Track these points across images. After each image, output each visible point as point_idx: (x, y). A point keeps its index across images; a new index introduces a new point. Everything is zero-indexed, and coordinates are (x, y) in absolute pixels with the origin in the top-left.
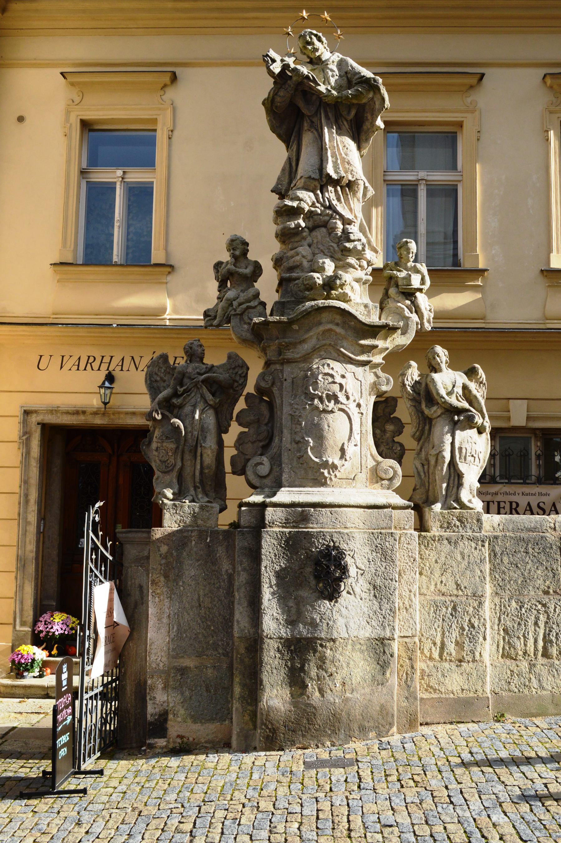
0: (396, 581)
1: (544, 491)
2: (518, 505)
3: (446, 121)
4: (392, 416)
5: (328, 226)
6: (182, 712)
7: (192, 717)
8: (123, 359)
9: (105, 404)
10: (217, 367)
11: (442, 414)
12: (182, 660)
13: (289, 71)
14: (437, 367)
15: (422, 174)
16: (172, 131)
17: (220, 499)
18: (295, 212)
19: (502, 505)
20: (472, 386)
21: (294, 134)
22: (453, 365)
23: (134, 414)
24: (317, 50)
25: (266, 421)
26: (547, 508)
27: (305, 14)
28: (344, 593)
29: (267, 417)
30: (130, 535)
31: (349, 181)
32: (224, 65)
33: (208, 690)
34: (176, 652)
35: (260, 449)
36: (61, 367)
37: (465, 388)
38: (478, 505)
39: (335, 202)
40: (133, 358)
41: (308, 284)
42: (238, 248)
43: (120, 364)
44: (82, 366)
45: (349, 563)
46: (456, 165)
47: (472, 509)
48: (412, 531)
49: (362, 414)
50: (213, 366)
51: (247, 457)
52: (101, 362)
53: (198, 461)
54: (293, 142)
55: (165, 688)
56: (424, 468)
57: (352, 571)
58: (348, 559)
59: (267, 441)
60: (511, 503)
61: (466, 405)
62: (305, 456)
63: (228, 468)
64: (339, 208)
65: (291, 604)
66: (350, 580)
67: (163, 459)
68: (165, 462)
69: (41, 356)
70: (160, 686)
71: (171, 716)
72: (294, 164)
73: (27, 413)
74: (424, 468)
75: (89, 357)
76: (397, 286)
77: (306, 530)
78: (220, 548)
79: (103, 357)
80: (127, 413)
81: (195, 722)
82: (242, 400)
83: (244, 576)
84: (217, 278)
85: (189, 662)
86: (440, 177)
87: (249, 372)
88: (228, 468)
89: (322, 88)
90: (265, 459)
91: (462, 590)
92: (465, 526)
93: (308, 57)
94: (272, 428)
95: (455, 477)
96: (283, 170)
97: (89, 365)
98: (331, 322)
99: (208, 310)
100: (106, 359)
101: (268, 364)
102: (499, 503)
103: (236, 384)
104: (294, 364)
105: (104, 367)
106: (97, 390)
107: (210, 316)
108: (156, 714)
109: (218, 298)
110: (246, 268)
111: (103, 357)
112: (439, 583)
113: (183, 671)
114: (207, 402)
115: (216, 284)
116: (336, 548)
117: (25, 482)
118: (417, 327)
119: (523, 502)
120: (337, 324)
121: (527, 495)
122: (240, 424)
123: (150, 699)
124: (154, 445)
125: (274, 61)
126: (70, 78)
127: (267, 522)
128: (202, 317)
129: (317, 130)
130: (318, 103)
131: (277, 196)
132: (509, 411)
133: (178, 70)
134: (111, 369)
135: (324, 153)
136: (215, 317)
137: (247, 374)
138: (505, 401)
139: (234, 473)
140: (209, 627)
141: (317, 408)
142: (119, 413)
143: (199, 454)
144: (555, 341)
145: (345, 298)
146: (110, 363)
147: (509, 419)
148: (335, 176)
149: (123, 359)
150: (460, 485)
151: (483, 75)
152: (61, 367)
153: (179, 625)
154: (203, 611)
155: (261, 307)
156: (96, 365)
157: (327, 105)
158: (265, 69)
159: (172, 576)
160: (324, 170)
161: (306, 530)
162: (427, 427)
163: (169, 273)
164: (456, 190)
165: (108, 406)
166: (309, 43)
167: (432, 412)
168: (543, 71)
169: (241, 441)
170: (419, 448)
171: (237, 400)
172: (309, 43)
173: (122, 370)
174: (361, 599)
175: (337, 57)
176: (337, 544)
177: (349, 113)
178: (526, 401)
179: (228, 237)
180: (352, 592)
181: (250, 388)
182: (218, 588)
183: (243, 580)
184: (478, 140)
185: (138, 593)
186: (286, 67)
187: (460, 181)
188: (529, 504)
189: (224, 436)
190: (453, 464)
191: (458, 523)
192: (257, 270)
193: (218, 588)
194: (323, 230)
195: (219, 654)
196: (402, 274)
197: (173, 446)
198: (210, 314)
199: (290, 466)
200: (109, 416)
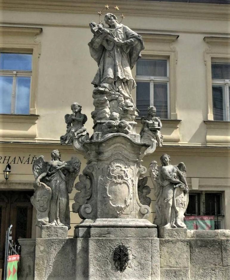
0: (150, 261)
3: (162, 55)
4: (145, 185)
5: (118, 100)
8: (15, 158)
9: (7, 179)
11: (168, 184)
13: (101, 31)
14: (166, 163)
15: (152, 78)
17: (67, 224)
18: (102, 93)
20: (181, 172)
21: (102, 58)
22: (172, 163)
23: (20, 183)
24: (114, 22)
25: (89, 188)
27: (107, 6)
28: (127, 268)
29: (89, 186)
31: (127, 80)
32: (64, 26)
35: (86, 201)
37: (178, 173)
38: (184, 225)
39: (121, 89)
41: (109, 125)
45: (129, 253)
46: (167, 74)
47: (183, 227)
48: (157, 238)
49: (133, 184)
51: (80, 204)
52: (5, 159)
53: (58, 206)
54: (101, 62)
56: (160, 209)
57: (131, 257)
58: (129, 252)
59: (89, 197)
61: (178, 180)
62: (108, 203)
63: (71, 209)
64: (123, 92)
66: (130, 261)
67: (41, 205)
68: (42, 207)
72: (102, 72)
74: (160, 209)
76: (148, 127)
77: (109, 238)
78: (68, 247)
79: (5, 157)
80: (16, 183)
82: (78, 178)
83: (80, 260)
84: (66, 122)
86: (159, 79)
87: (81, 165)
88: (71, 209)
89: (116, 39)
90: (89, 205)
91: (179, 265)
92: (179, 235)
93: (109, 25)
94: (92, 191)
95: (175, 213)
96: (97, 75)
99: (63, 136)
100: (7, 158)
101: (89, 162)
103: (76, 171)
104: (103, 162)
105: (6, 161)
106: (3, 173)
107: (63, 139)
109: (67, 131)
110: (80, 117)
111: (5, 157)
112: (168, 262)
114: (62, 179)
115: (66, 125)
116: (123, 246)
118: (157, 146)
122: (77, 189)
124: (37, 199)
125: (94, 26)
127: (91, 235)
128: (60, 140)
129: (112, 57)
130: (113, 45)
131: (94, 86)
132: (191, 183)
133: (43, 28)
134: (9, 163)
135: (116, 67)
137: (80, 166)
138: (189, 178)
139: (74, 212)
141: (114, 182)
142: (13, 183)
143: (58, 203)
145: (127, 133)
146: (9, 160)
148: (121, 78)
149: (15, 158)
150: (176, 216)
151: (178, 36)
157: (118, 46)
158: (90, 30)
160: (116, 75)
161: (109, 238)
162: (161, 190)
164: (166, 86)
165: (8, 180)
166: (109, 19)
167: (166, 183)
168: (203, 36)
169: (76, 198)
170: (158, 200)
171: (75, 178)
172: (109, 19)
173: (14, 163)
174: (135, 270)
175: (121, 25)
176: (124, 245)
177: (127, 50)
178: (198, 178)
180: (130, 267)
181: (81, 173)
182: (68, 266)
183: (80, 262)
184: (206, 65)
186: (100, 29)
187: (168, 81)
189: (69, 194)
190: (173, 207)
191: (176, 234)
192: (85, 119)
193: (68, 266)
194: (115, 101)
196: (151, 122)
198: (64, 138)
199: (101, 209)
200: (8, 185)
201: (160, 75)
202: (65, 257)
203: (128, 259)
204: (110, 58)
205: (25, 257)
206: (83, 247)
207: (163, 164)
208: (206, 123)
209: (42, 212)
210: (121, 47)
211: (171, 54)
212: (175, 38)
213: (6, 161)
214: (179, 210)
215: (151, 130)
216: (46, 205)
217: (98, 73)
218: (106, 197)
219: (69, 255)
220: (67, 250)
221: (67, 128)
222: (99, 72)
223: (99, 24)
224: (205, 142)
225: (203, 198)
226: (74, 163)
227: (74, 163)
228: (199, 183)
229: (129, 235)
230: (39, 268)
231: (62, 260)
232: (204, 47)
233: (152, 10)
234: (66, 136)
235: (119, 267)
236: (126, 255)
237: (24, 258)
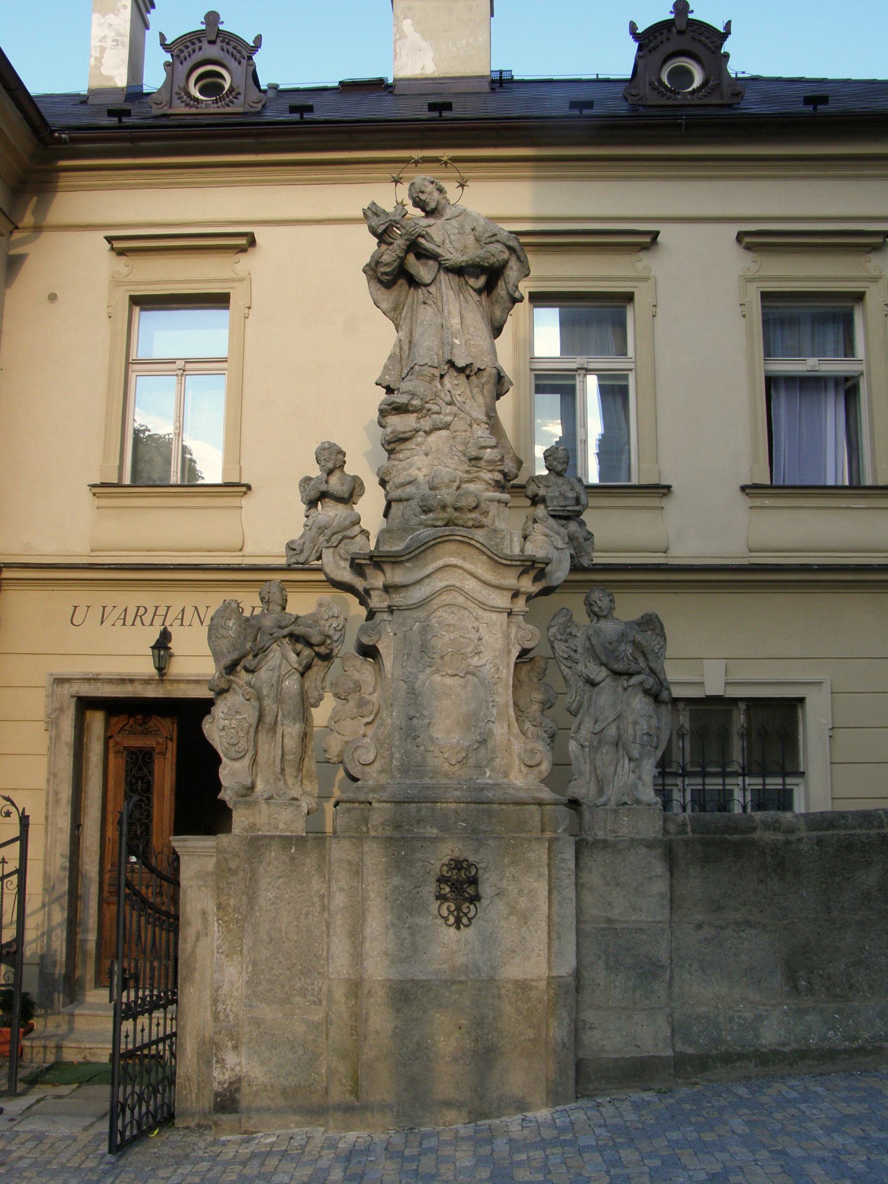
8: (183, 610)
10: (304, 617)
11: (607, 676)
23: (197, 682)
30: (186, 844)
36: (102, 622)
40: (196, 608)
42: (332, 458)
43: (180, 617)
44: (129, 621)
50: (298, 617)
52: (155, 615)
65: (405, 934)
66: (484, 902)
67: (232, 741)
69: (76, 607)
72: (406, 348)
73: (60, 681)
75: (138, 608)
96: (391, 357)
97: (138, 618)
99: (292, 542)
100: (162, 611)
105: (158, 620)
107: (294, 550)
108: (225, 1082)
111: (157, 607)
117: (53, 775)
123: (217, 1062)
136: (302, 551)
144: (217, 508)
146: (166, 616)
149: (183, 610)
151: (657, 233)
152: (102, 622)
155: (364, 537)
156: (147, 619)
163: (245, 493)
179: (315, 446)
184: (654, 316)
185: (199, 921)
187: (631, 370)
195: (309, 1001)
201: (602, 351)
202: (299, 887)
204: (430, 305)
205: (191, 887)
207: (592, 616)
208: (748, 491)
209: (235, 760)
212: (647, 239)
213: (158, 620)
215: (554, 516)
216: (245, 739)
217: (394, 353)
218: (417, 715)
219: (311, 882)
220: (306, 870)
221: (307, 517)
222: (398, 351)
223: (390, 197)
224: (747, 550)
225: (740, 719)
226: (327, 620)
227: (327, 620)
228: (726, 675)
230: (226, 918)
231: (291, 897)
232: (739, 262)
234: (301, 541)
235: (452, 920)
237: (189, 890)
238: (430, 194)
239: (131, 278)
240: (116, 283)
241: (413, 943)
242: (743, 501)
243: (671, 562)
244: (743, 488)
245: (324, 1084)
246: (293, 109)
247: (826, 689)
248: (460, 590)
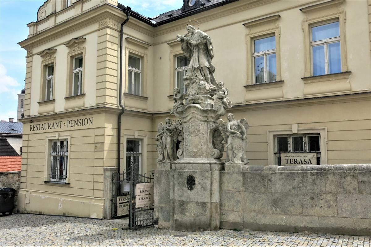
1: (306, 156)
2: (297, 160)
6: (162, 218)
7: (164, 220)
12: (161, 205)
16: (280, 34)
19: (292, 160)
26: (307, 161)
33: (167, 213)
34: (160, 203)
55: (158, 212)
57: (196, 182)
58: (195, 179)
60: (295, 160)
65: (181, 191)
66: (196, 185)
70: (157, 211)
71: (159, 219)
81: (165, 221)
85: (163, 205)
98: (194, 110)
102: (291, 159)
113: (162, 208)
119: (299, 159)
120: (196, 111)
121: (300, 157)
126: (246, 26)
140: (167, 196)
147: (292, 131)
153: (161, 195)
154: (166, 192)
159: (159, 182)
178: (297, 125)
184: (345, 22)
188: (301, 160)
197: (160, 147)
203: (195, 184)
206: (49, 174)
210: (197, 46)
211: (276, 30)
214: (237, 152)
229: (196, 169)
233: (174, 26)
236: (194, 181)
238: (190, 29)
239: (251, 33)
240: (171, 53)
241: (183, 193)
242: (302, 82)
243: (284, 100)
244: (302, 78)
245: (299, 217)
246: (169, 16)
247: (326, 130)
248: (195, 117)
